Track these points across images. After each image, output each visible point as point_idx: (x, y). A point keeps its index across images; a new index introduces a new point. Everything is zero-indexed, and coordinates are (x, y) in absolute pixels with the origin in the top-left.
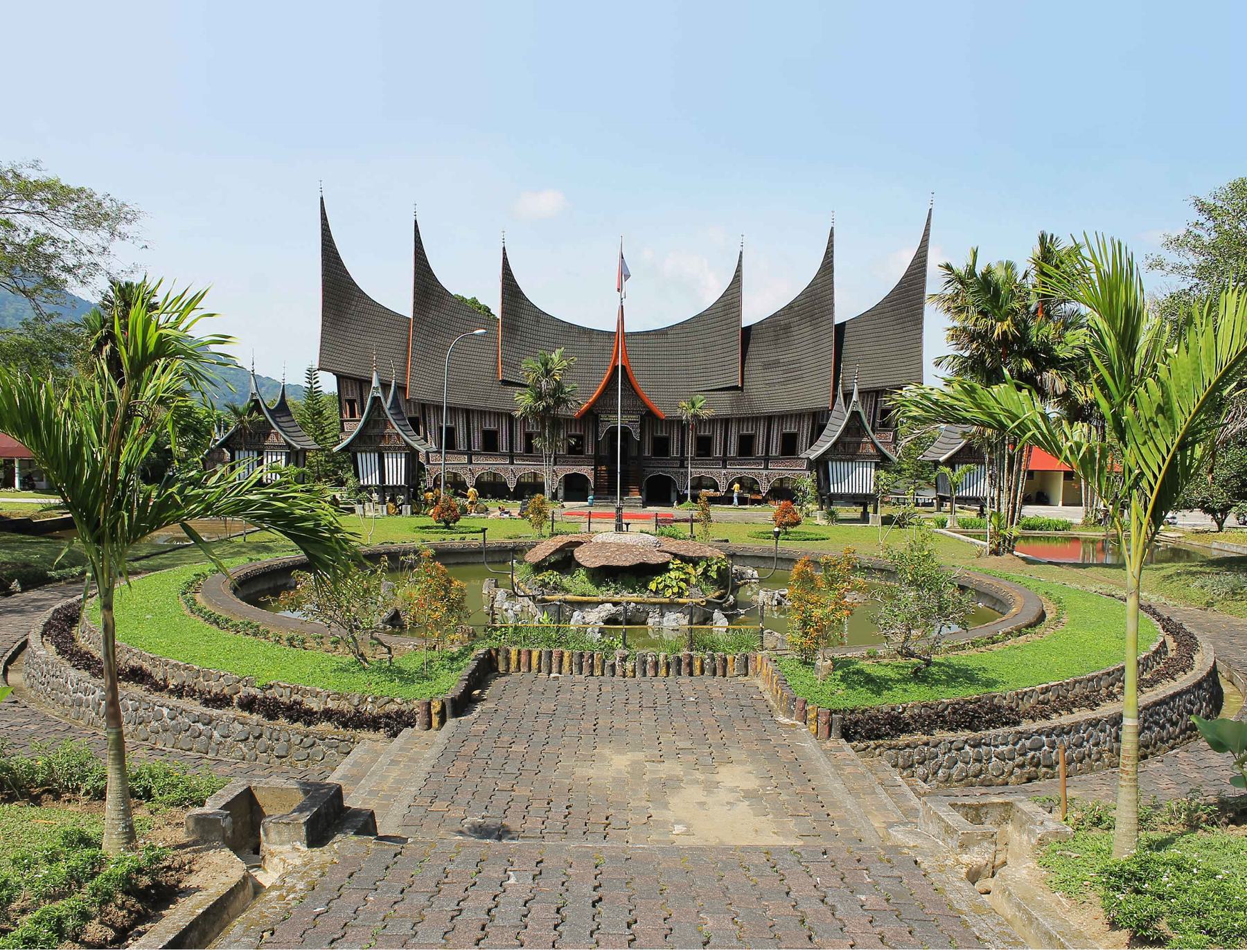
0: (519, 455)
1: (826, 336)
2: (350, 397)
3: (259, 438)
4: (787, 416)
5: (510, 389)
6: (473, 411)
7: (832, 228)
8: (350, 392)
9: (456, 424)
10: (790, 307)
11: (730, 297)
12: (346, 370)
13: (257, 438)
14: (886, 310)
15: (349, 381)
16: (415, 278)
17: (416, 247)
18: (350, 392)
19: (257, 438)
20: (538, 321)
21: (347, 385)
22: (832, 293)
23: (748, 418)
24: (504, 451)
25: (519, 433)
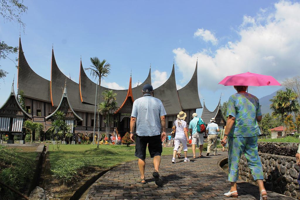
0: (89, 127)
1: (176, 94)
2: (28, 105)
3: (12, 112)
4: (170, 116)
5: (86, 105)
6: (89, 113)
7: (174, 64)
8: (28, 104)
10: (163, 85)
11: (148, 81)
12: (26, 94)
13: (11, 112)
14: (188, 88)
15: (28, 100)
16: (52, 67)
17: (52, 57)
18: (28, 104)
19: (11, 112)
20: (91, 85)
21: (27, 101)
22: (175, 82)
23: (80, 112)
24: (84, 126)
25: (89, 120)
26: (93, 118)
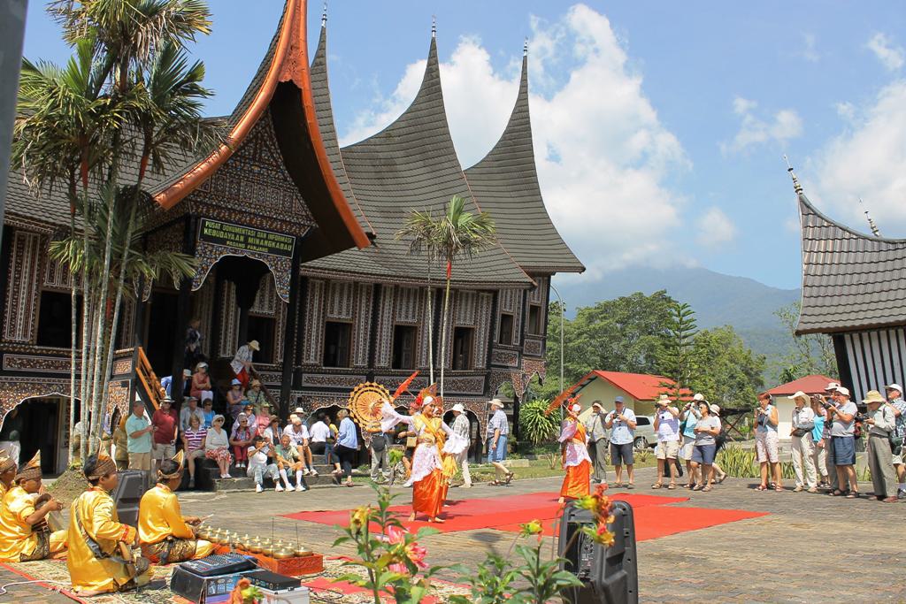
9: (354, 318)
26: (52, 279)
